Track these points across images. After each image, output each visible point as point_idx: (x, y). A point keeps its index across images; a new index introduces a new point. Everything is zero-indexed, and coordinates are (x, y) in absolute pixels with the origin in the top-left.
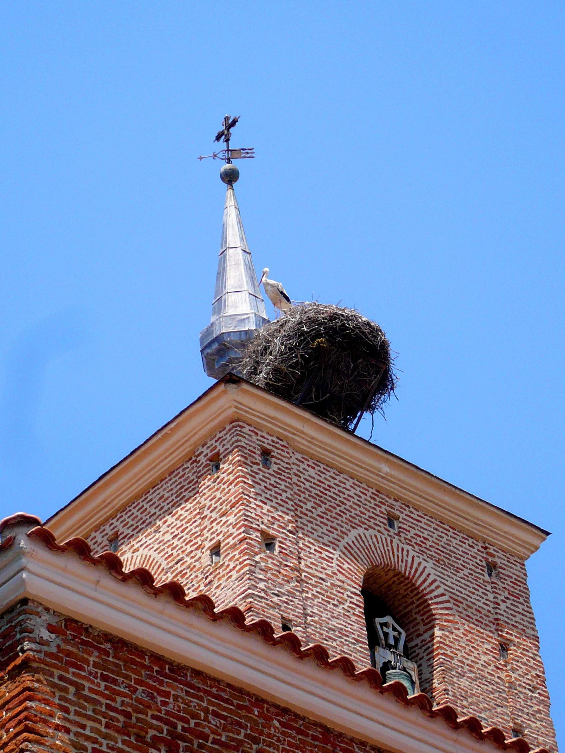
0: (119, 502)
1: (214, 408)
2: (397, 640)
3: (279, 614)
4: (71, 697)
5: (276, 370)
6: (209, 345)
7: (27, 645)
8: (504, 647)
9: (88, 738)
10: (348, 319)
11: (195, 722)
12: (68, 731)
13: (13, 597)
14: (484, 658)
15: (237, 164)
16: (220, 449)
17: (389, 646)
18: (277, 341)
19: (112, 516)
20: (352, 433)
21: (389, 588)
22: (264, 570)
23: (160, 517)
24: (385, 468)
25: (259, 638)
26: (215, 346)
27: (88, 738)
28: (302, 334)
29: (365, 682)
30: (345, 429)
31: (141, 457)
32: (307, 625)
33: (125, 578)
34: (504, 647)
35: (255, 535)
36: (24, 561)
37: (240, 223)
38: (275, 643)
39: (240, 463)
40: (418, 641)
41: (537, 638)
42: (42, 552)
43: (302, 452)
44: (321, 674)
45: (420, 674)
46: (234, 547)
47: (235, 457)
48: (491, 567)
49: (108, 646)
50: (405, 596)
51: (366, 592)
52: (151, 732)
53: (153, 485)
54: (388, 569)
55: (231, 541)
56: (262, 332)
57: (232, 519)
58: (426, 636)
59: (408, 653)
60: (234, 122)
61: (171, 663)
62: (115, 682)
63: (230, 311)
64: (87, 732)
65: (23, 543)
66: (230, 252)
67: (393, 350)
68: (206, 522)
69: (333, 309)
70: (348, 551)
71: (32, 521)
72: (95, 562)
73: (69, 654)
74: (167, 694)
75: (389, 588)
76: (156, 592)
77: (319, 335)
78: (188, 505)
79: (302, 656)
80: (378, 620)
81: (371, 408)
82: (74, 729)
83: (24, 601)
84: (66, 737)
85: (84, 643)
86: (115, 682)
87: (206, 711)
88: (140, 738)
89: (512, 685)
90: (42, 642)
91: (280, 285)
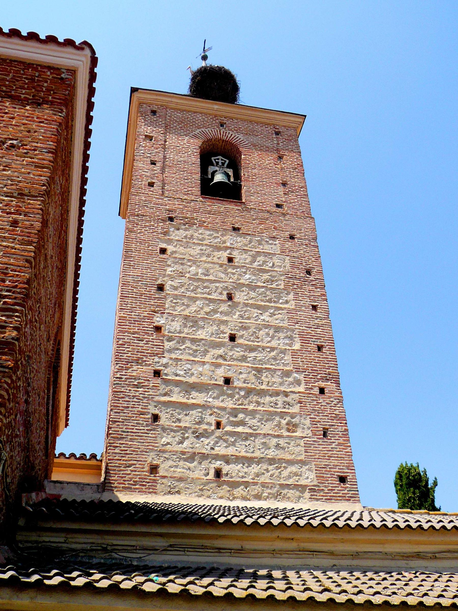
1: (134, 106)
3: (315, 345)
11: (73, 72)
21: (224, 149)
25: (70, 47)
41: (300, 152)
43: (172, 109)
50: (231, 149)
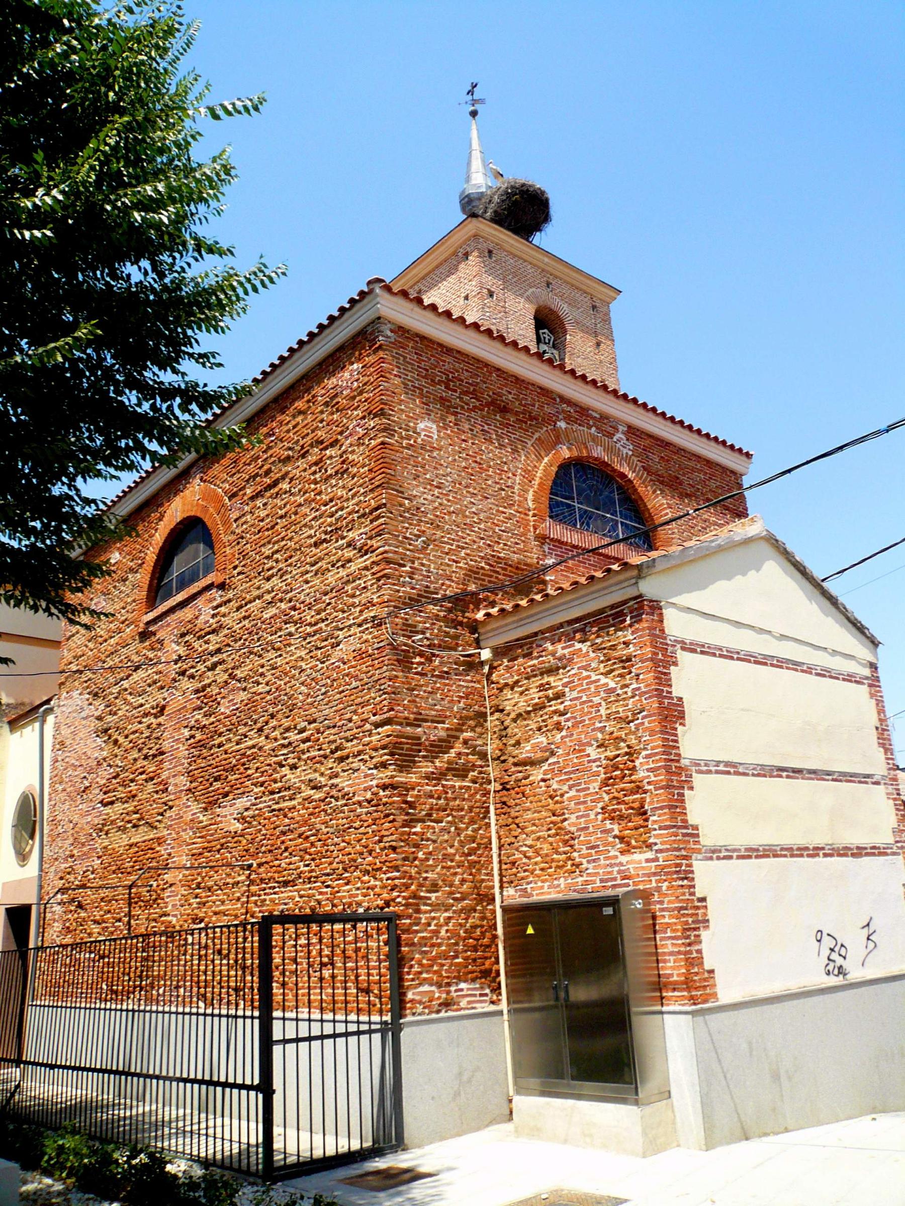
0: (421, 275)
1: (466, 229)
2: (549, 340)
4: (401, 361)
5: (495, 212)
6: (463, 199)
7: (381, 338)
8: (598, 344)
9: (409, 380)
10: (530, 186)
12: (400, 377)
13: (373, 317)
14: (589, 349)
15: (478, 107)
16: (469, 249)
17: (546, 343)
18: (496, 197)
19: (418, 282)
20: (531, 242)
21: (547, 316)
22: (489, 307)
23: (440, 282)
24: (546, 260)
26: (466, 199)
27: (409, 380)
28: (508, 193)
29: (535, 357)
30: (528, 240)
31: (431, 254)
32: (508, 333)
33: (425, 308)
34: (598, 344)
35: (485, 291)
36: (378, 299)
37: (479, 137)
38: (494, 339)
39: (478, 257)
40: (559, 341)
41: (613, 340)
42: (387, 295)
44: (515, 353)
45: (560, 356)
46: (475, 296)
47: (476, 253)
48: (594, 307)
49: (417, 339)
51: (535, 318)
52: (438, 378)
53: (437, 267)
54: (546, 307)
55: (474, 293)
56: (489, 192)
57: (474, 283)
58: (563, 339)
59: (554, 347)
60: (476, 85)
61: (446, 347)
62: (421, 355)
63: (473, 182)
64: (409, 378)
65: (378, 291)
66: (474, 152)
67: (551, 202)
68: (462, 285)
69: (523, 181)
70: (528, 299)
71: (382, 281)
72: (411, 300)
73: (400, 342)
74: (444, 361)
75: (547, 316)
76: (440, 314)
77: (516, 194)
78: (453, 276)
79: (507, 345)
80: (541, 331)
81: (540, 230)
82: (403, 376)
83: (379, 318)
84: (399, 380)
85: (406, 337)
86: (421, 355)
87: (463, 369)
88: (433, 381)
89: (601, 362)
90: (388, 337)
91: (499, 169)
